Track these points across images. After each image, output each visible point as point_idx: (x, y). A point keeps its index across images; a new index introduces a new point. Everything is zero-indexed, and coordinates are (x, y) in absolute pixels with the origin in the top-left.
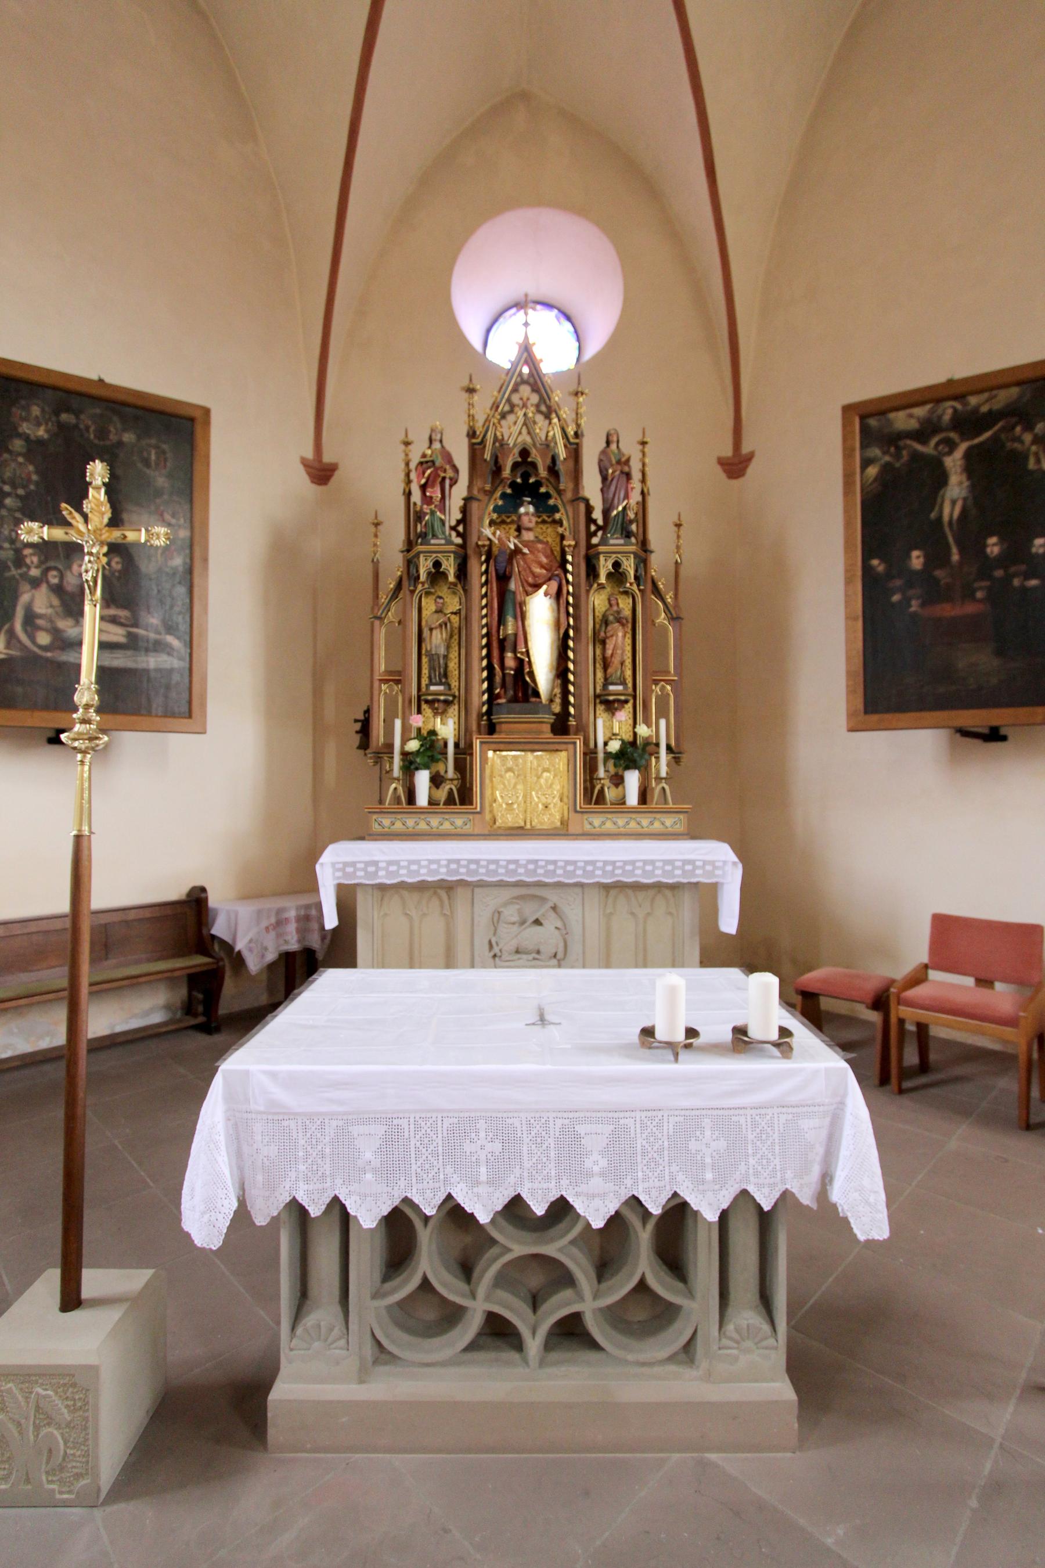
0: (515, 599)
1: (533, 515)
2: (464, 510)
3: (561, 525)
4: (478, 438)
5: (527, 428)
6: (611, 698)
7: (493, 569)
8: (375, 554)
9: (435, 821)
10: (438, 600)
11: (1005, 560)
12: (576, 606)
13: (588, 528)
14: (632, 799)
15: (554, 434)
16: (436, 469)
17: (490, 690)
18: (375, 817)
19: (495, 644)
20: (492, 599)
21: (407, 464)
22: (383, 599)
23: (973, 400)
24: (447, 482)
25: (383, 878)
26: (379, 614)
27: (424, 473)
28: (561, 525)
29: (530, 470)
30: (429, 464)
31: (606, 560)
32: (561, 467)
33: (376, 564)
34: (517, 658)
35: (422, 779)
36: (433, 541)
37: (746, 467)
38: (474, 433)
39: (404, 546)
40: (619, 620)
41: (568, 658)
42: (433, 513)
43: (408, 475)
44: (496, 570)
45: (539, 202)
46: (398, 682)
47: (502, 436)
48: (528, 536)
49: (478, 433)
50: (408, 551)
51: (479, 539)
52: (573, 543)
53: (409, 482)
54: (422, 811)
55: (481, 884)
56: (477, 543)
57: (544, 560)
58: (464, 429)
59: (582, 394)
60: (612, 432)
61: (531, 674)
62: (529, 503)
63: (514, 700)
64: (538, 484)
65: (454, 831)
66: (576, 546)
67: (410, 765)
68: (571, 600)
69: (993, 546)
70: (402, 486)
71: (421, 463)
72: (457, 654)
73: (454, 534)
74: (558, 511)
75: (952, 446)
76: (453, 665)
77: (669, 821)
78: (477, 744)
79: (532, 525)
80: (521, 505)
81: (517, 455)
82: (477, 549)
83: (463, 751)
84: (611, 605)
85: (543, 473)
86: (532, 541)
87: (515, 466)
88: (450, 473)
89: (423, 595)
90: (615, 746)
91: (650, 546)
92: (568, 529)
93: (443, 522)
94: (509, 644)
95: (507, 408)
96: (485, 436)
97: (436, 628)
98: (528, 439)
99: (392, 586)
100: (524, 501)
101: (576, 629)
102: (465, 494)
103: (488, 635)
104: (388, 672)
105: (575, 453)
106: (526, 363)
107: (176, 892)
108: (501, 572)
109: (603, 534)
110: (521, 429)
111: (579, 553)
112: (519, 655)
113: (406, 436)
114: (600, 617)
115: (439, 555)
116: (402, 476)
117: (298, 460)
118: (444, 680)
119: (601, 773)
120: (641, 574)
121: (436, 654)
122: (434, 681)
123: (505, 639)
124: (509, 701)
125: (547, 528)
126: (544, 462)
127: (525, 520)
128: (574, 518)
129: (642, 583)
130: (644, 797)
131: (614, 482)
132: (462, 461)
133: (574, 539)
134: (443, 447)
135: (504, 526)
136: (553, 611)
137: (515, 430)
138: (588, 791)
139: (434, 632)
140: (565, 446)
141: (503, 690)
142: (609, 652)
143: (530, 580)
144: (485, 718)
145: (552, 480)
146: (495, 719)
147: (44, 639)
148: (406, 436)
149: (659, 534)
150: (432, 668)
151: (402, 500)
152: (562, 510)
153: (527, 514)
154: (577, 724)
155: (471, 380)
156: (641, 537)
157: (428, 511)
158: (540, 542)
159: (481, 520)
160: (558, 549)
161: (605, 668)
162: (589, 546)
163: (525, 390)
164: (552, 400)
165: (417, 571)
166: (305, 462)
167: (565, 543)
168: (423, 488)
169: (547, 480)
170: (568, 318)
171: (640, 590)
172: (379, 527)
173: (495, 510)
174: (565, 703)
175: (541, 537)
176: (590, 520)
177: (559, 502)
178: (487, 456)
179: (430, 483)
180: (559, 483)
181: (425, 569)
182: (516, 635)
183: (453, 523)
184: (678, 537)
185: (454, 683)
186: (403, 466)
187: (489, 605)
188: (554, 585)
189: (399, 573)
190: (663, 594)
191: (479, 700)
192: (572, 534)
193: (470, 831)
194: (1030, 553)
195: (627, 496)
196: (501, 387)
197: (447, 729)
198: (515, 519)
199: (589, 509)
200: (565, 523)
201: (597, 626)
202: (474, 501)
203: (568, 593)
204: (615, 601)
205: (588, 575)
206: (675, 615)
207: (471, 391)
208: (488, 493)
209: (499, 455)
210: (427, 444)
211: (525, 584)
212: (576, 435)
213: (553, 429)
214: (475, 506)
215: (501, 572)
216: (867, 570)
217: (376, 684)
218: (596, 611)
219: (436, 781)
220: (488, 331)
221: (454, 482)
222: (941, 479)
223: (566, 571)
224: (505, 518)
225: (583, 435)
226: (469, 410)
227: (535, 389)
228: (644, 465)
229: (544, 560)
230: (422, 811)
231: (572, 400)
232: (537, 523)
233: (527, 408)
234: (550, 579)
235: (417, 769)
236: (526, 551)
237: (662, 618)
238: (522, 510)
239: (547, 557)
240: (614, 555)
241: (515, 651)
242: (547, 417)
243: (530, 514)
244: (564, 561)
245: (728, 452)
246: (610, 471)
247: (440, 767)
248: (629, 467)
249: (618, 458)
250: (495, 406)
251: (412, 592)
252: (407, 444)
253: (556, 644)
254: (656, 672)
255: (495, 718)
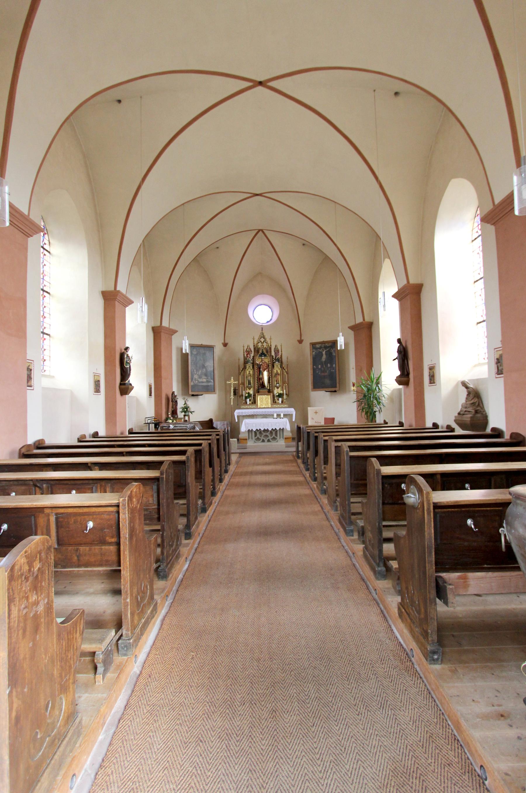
9: (250, 406)
11: (330, 367)
14: (280, 402)
22: (240, 371)
23: (326, 344)
25: (244, 414)
35: (248, 400)
45: (263, 293)
54: (248, 405)
55: (258, 415)
63: (262, 387)
67: (246, 398)
69: (329, 365)
70: (243, 354)
75: (323, 351)
77: (286, 405)
78: (256, 395)
83: (254, 395)
90: (277, 394)
104: (241, 383)
105: (270, 348)
107: (207, 419)
119: (275, 398)
130: (282, 402)
132: (253, 350)
138: (273, 401)
147: (197, 382)
149: (284, 359)
151: (243, 356)
161: (276, 381)
168: (247, 355)
174: (270, 388)
176: (273, 358)
185: (252, 385)
194: (73, 489)
197: (251, 392)
216: (313, 367)
219: (250, 400)
222: (322, 355)
230: (248, 405)
237: (285, 373)
244: (269, 366)
247: (250, 398)
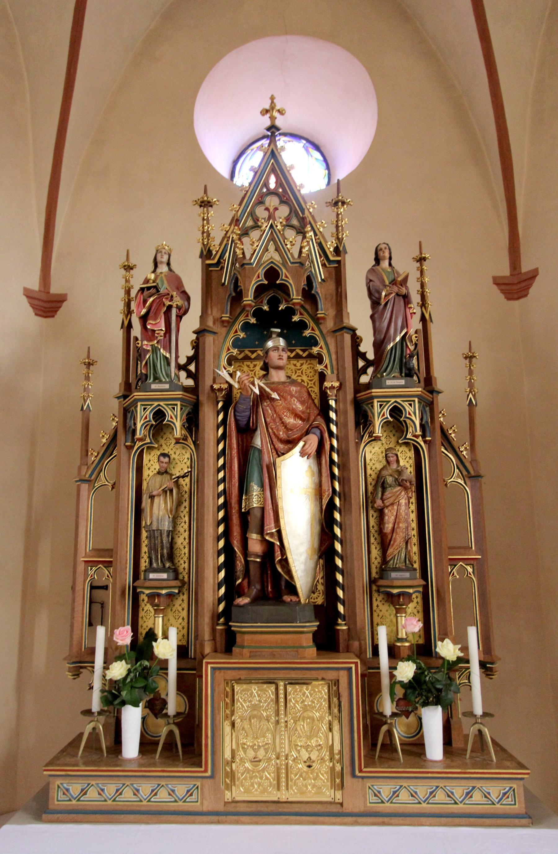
0: (261, 459)
1: (283, 350)
2: (196, 345)
3: (321, 362)
4: (213, 259)
5: (400, 788)
6: (395, 591)
7: (233, 419)
8: (85, 401)
9: (145, 788)
10: (162, 459)
12: (343, 466)
13: (355, 363)
15: (310, 250)
16: (161, 296)
17: (229, 580)
18: (58, 782)
19: (235, 520)
20: (231, 459)
21: (128, 292)
24: (174, 312)
26: (87, 476)
27: (145, 302)
28: (321, 362)
29: (280, 295)
30: (152, 291)
31: (381, 406)
32: (319, 290)
33: (86, 413)
34: (264, 540)
36: (153, 386)
37: (528, 287)
38: (210, 252)
39: (120, 391)
40: (400, 483)
41: (334, 536)
42: (155, 350)
43: (128, 305)
44: (236, 421)
46: (108, 564)
47: (243, 253)
48: (278, 376)
49: (214, 253)
50: (125, 397)
51: (214, 382)
52: (337, 384)
53: (129, 312)
56: (212, 387)
57: (299, 407)
58: (198, 248)
59: (343, 203)
60: (383, 246)
61: (285, 562)
62: (279, 335)
64: (290, 311)
65: (173, 806)
66: (340, 388)
68: (335, 457)
70: (119, 318)
71: (142, 290)
72: (186, 526)
73: (183, 374)
74: (316, 344)
76: (181, 541)
79: (281, 363)
80: (269, 337)
81: (262, 277)
82: (212, 395)
84: (388, 462)
85: (296, 297)
86: (284, 383)
87: (260, 290)
88: (178, 301)
89: (145, 451)
91: (436, 385)
92: (329, 366)
93: (168, 361)
94: (253, 521)
95: (250, 223)
96: (222, 256)
97: (159, 495)
98: (277, 257)
99: (104, 441)
100: (272, 332)
101: (345, 496)
102: (196, 325)
103: (226, 506)
106: (273, 171)
108: (243, 422)
109: (374, 372)
110: (491, 801)
111: (345, 397)
112: (267, 538)
113: (128, 259)
114: (374, 476)
115: (161, 403)
116: (121, 306)
117: (22, 291)
118: (168, 565)
120: (427, 422)
121: (158, 530)
122: (155, 565)
123: (248, 513)
124: (255, 601)
125: (302, 365)
126: (297, 283)
127: (274, 356)
128: (337, 353)
129: (428, 433)
131: (389, 306)
133: (338, 380)
134: (170, 270)
135: (249, 363)
136: (313, 475)
137: (259, 246)
139: (156, 500)
140: (324, 265)
141: (246, 581)
142: (388, 527)
143: (282, 434)
144: (222, 620)
145: (308, 307)
146: (235, 626)
148: (128, 259)
150: (152, 548)
151: (120, 334)
152: (322, 343)
153: (276, 348)
154: (349, 629)
155: (205, 192)
156: (423, 374)
157: (149, 348)
158: (294, 383)
159: (217, 357)
160: (316, 389)
161: (384, 545)
162: (359, 388)
163: (272, 202)
164: (306, 212)
165: (135, 424)
166: (29, 294)
167: (327, 384)
168: (144, 319)
169: (302, 306)
170: (317, 148)
171: (425, 442)
172: (91, 367)
173: (235, 345)
175: (294, 377)
176: (357, 354)
177: (317, 332)
178: (225, 279)
179: (151, 314)
180: (317, 310)
181: (142, 422)
182: (263, 509)
183: (182, 361)
184: (471, 372)
185: (183, 565)
186: (122, 293)
187: (227, 465)
188: (313, 440)
189: (114, 424)
190: (456, 445)
191: (214, 595)
192: (335, 372)
193: (197, 807)
195: (405, 324)
196: (243, 199)
198: (261, 353)
199: (356, 341)
200: (326, 360)
201: (370, 488)
202: (207, 334)
203: (332, 447)
204: (395, 457)
205: (357, 425)
206: (472, 473)
207: (206, 204)
208: (226, 324)
209: (239, 277)
210: (152, 267)
211: (275, 440)
212: (337, 251)
213: (308, 244)
214: (209, 339)
215: (243, 422)
217: (81, 567)
218: (368, 467)
220: (235, 162)
221: (183, 312)
223: (328, 420)
224: (250, 354)
225: (346, 252)
226: (203, 226)
227: (284, 201)
228: (422, 286)
229: (299, 407)
231: (331, 213)
232: (289, 357)
233: (275, 219)
234: (307, 433)
235: (124, 703)
236: (275, 395)
237: (456, 478)
238: (270, 344)
239: (302, 403)
240: (393, 400)
241: (261, 531)
242: (301, 232)
243: (281, 348)
244: (324, 409)
245: (504, 270)
246: (384, 294)
248: (407, 288)
249: (391, 278)
250: (235, 221)
251: (130, 448)
252: (128, 268)
253: (318, 515)
254: (454, 548)
255: (235, 626)
